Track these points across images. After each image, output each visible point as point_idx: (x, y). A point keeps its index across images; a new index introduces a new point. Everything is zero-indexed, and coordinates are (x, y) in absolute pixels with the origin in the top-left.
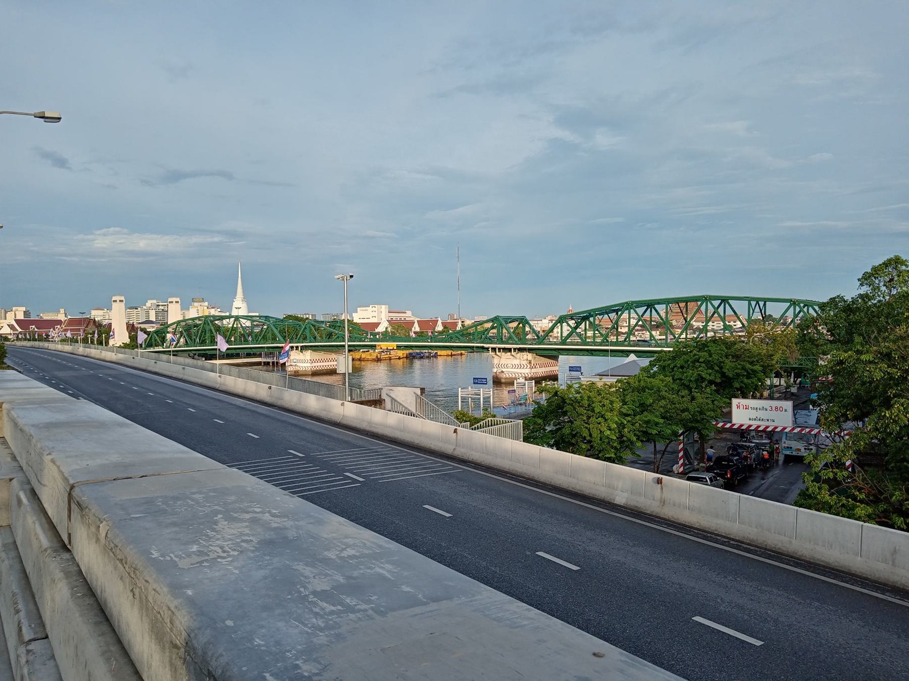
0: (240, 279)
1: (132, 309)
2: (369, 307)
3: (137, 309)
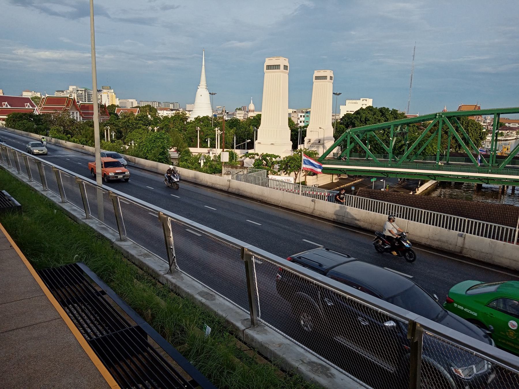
0: (203, 67)
1: (59, 92)
2: (360, 100)
3: (63, 92)
